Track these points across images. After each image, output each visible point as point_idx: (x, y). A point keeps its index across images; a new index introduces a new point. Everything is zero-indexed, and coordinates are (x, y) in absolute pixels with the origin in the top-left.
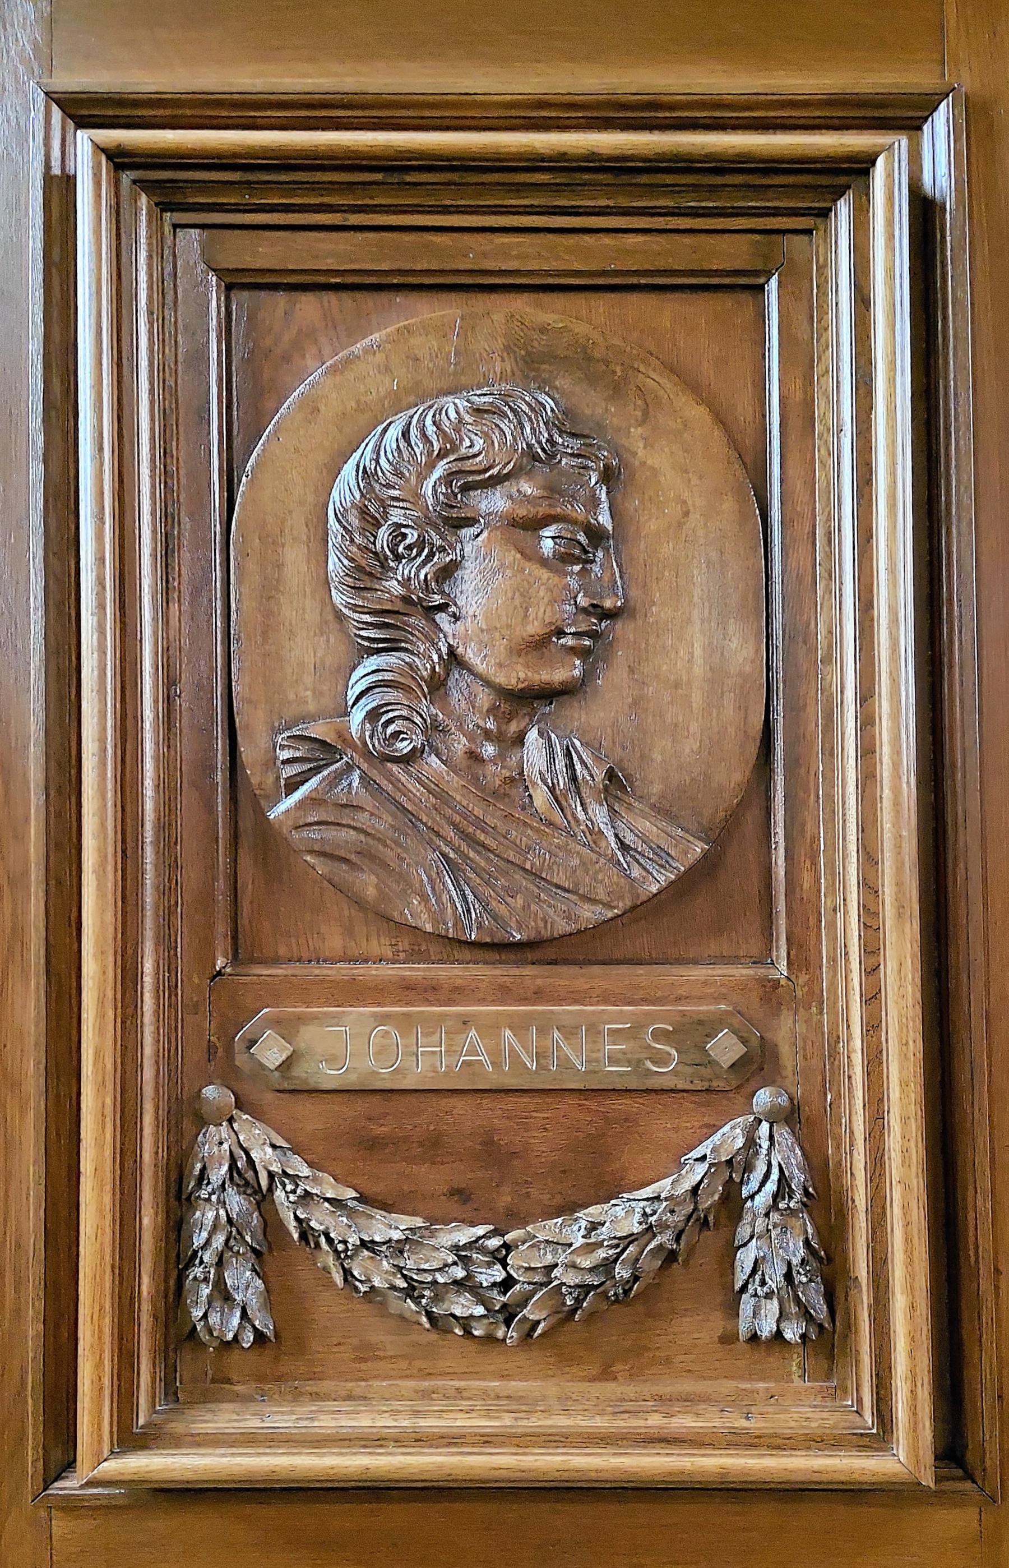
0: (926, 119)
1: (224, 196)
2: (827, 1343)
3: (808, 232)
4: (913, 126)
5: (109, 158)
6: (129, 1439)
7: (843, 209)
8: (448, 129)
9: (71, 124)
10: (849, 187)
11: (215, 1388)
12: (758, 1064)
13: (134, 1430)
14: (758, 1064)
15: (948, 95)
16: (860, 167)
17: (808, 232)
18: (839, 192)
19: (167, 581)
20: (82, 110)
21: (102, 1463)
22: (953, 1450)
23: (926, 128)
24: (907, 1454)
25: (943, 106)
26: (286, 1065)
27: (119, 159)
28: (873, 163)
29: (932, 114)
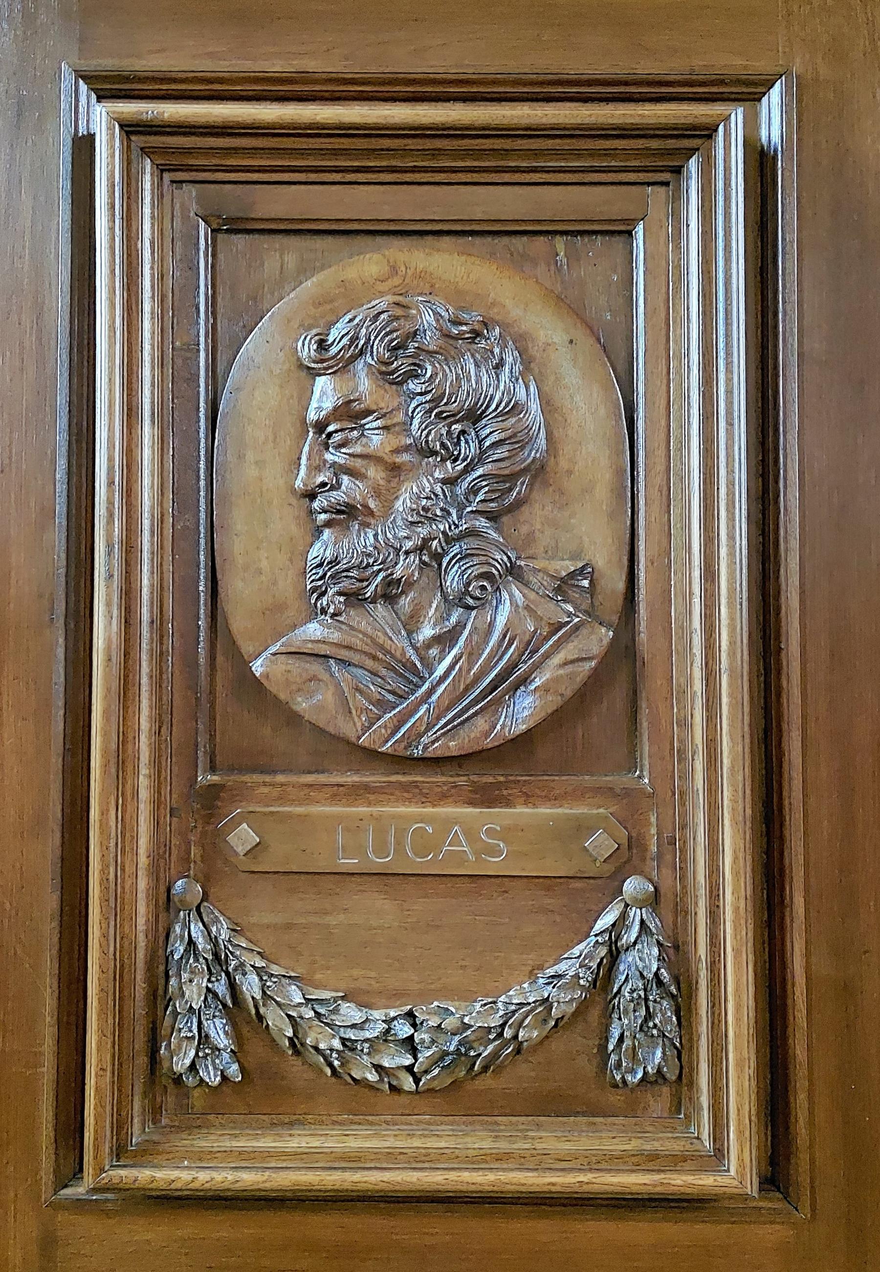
0: (765, 94)
1: (547, 814)
2: (677, 1082)
3: (667, 184)
4: (757, 98)
5: (121, 126)
6: (121, 1152)
7: (693, 164)
8: (549, 99)
9: (94, 96)
10: (698, 149)
11: (192, 1121)
12: (628, 858)
13: (130, 1148)
14: (628, 858)
15: (781, 76)
16: (707, 132)
17: (667, 184)
18: (690, 152)
19: (162, 573)
20: (109, 87)
21: (102, 1170)
22: (776, 1173)
23: (765, 99)
24: (737, 1171)
25: (778, 84)
26: (254, 851)
27: (130, 129)
28: (716, 130)
29: (769, 90)
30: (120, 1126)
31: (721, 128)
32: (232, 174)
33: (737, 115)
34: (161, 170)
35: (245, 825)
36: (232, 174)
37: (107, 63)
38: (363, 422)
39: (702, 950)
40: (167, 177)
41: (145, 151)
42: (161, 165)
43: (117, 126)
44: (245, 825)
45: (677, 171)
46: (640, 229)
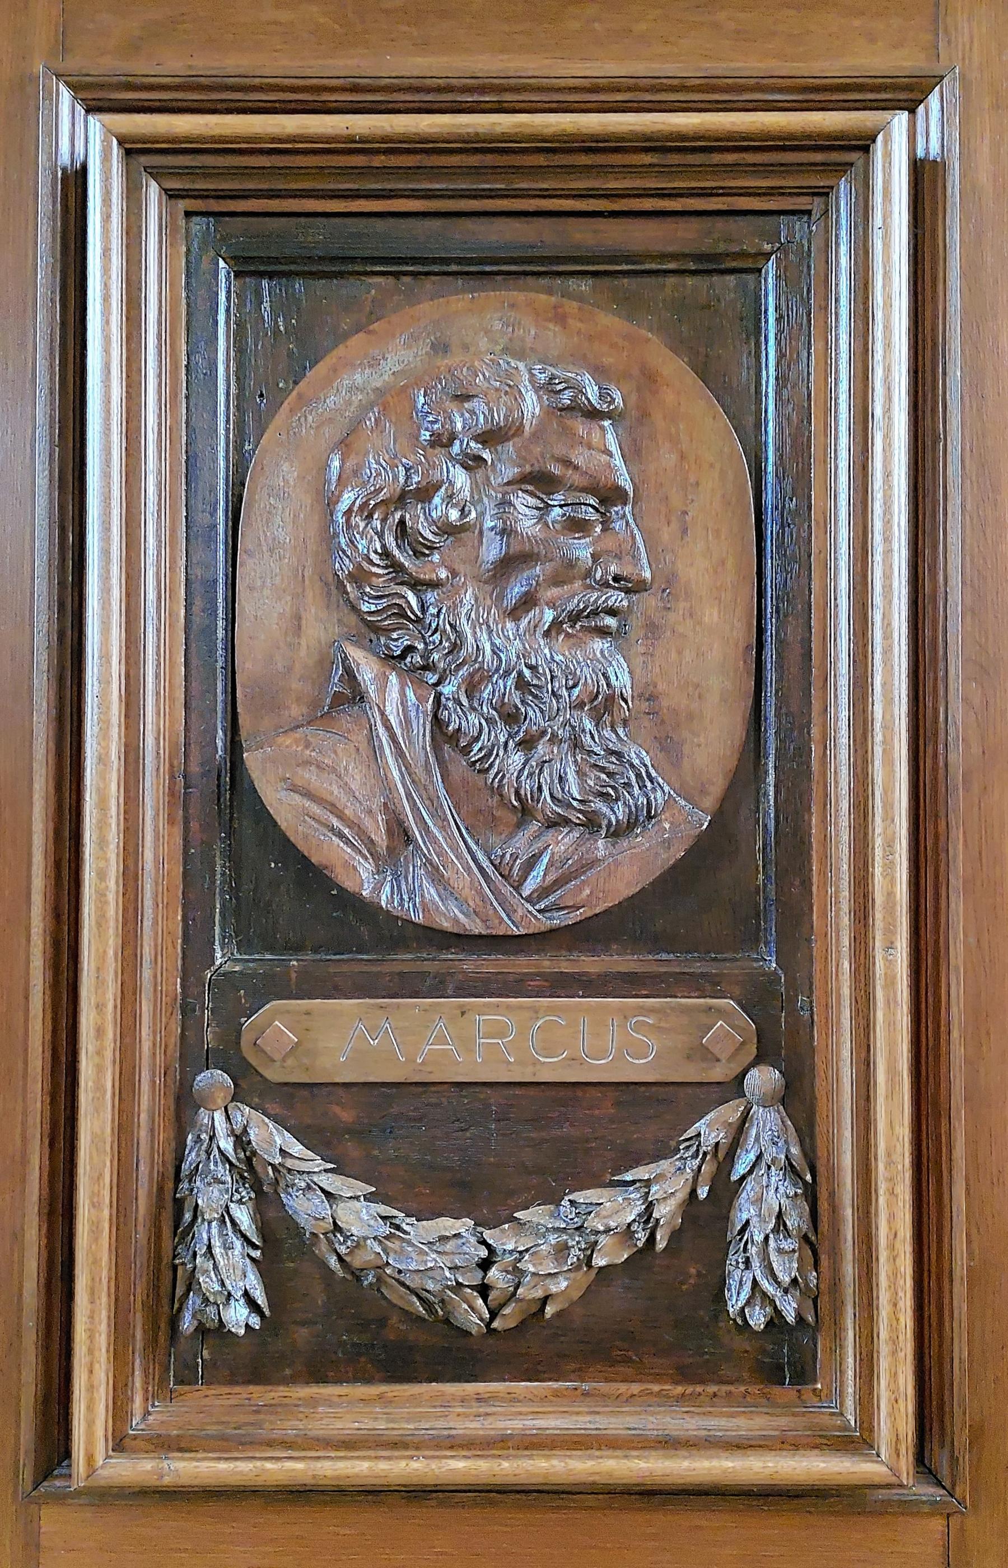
0: (922, 101)
16: (863, 144)
27: (132, 149)
28: (874, 141)
30: (119, 1410)
31: (880, 138)
32: (306, 233)
33: (900, 120)
34: (172, 195)
35: (277, 1022)
36: (306, 233)
37: (107, 65)
38: (499, 1208)
39: (847, 1160)
40: (182, 205)
41: (155, 173)
42: (171, 190)
43: (115, 142)
44: (277, 1022)
45: (824, 193)
46: (771, 268)
